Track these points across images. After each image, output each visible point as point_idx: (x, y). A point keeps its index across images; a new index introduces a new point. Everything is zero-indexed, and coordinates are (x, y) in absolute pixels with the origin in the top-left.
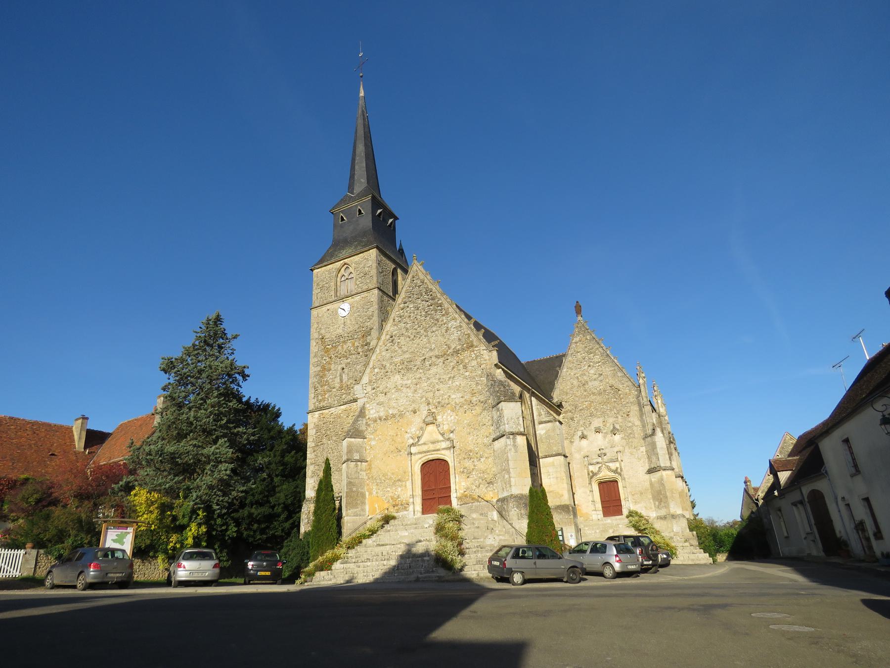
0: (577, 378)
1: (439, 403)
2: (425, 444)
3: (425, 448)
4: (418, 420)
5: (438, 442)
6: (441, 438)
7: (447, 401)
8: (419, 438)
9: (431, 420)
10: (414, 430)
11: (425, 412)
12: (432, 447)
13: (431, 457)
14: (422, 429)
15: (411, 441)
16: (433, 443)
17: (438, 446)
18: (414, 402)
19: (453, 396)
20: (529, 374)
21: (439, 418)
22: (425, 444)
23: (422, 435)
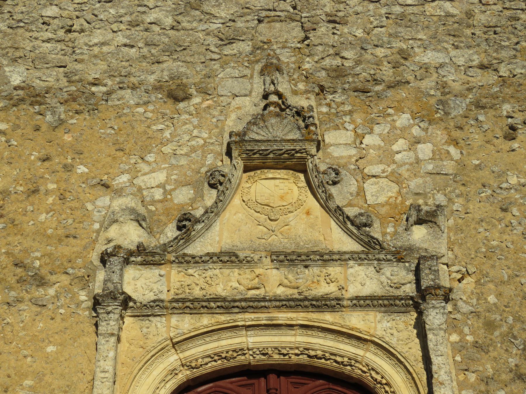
0: (118, 46)
1: (338, 73)
2: (229, 258)
3: (227, 282)
4: (196, 136)
5: (327, 258)
6: (341, 241)
7: (387, 72)
8: (186, 224)
9: (276, 149)
10: (157, 180)
11: (249, 105)
12: (276, 281)
13: (256, 343)
14: (216, 181)
15: (131, 235)
16: (289, 259)
17: (320, 282)
18: (175, 49)
19: (430, 57)
20: (154, 264)
21: (338, 144)
22: (229, 258)
23: (214, 212)
